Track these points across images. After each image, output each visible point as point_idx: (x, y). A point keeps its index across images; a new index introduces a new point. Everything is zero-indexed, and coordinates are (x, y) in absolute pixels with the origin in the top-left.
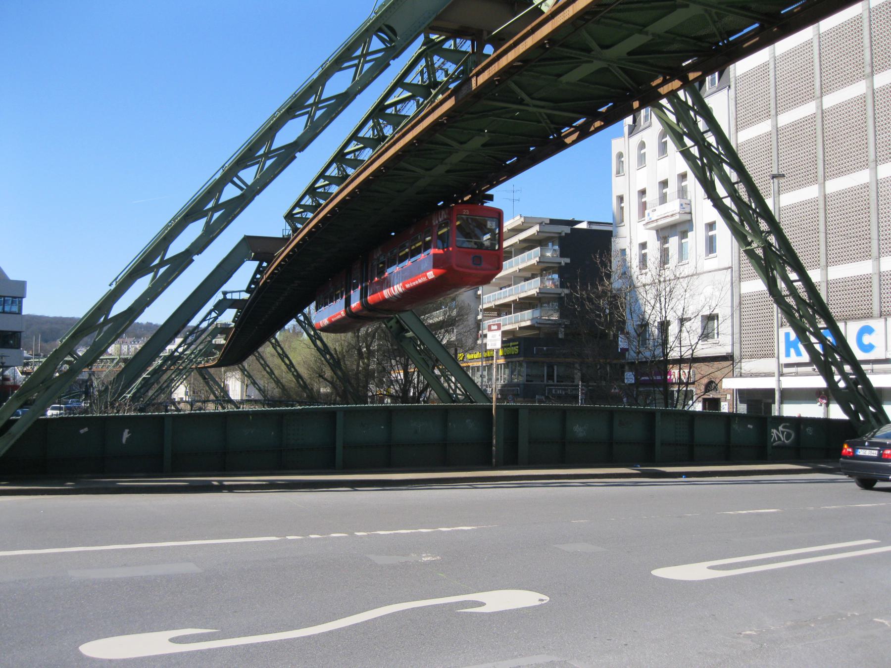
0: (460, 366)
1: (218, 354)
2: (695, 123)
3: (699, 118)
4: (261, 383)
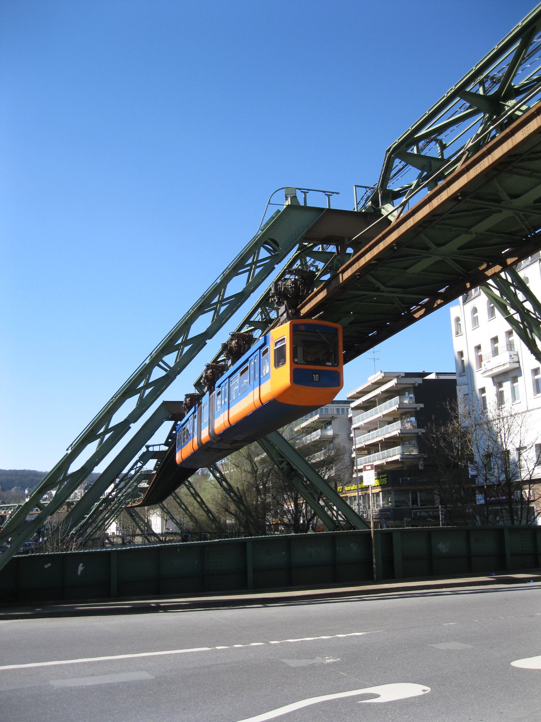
0: (340, 497)
1: (143, 496)
2: (515, 295)
3: (518, 292)
4: (177, 517)
